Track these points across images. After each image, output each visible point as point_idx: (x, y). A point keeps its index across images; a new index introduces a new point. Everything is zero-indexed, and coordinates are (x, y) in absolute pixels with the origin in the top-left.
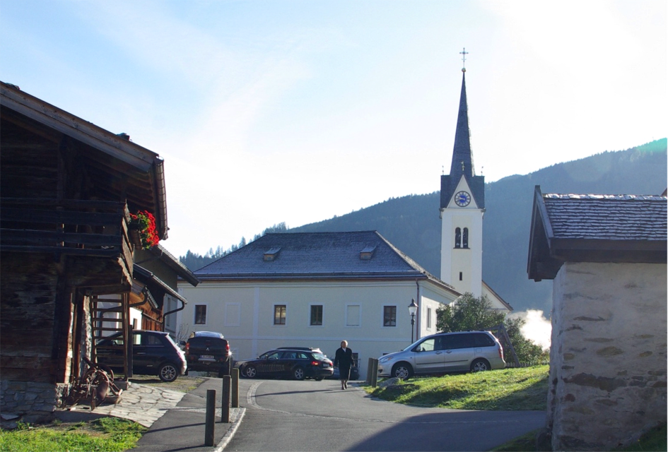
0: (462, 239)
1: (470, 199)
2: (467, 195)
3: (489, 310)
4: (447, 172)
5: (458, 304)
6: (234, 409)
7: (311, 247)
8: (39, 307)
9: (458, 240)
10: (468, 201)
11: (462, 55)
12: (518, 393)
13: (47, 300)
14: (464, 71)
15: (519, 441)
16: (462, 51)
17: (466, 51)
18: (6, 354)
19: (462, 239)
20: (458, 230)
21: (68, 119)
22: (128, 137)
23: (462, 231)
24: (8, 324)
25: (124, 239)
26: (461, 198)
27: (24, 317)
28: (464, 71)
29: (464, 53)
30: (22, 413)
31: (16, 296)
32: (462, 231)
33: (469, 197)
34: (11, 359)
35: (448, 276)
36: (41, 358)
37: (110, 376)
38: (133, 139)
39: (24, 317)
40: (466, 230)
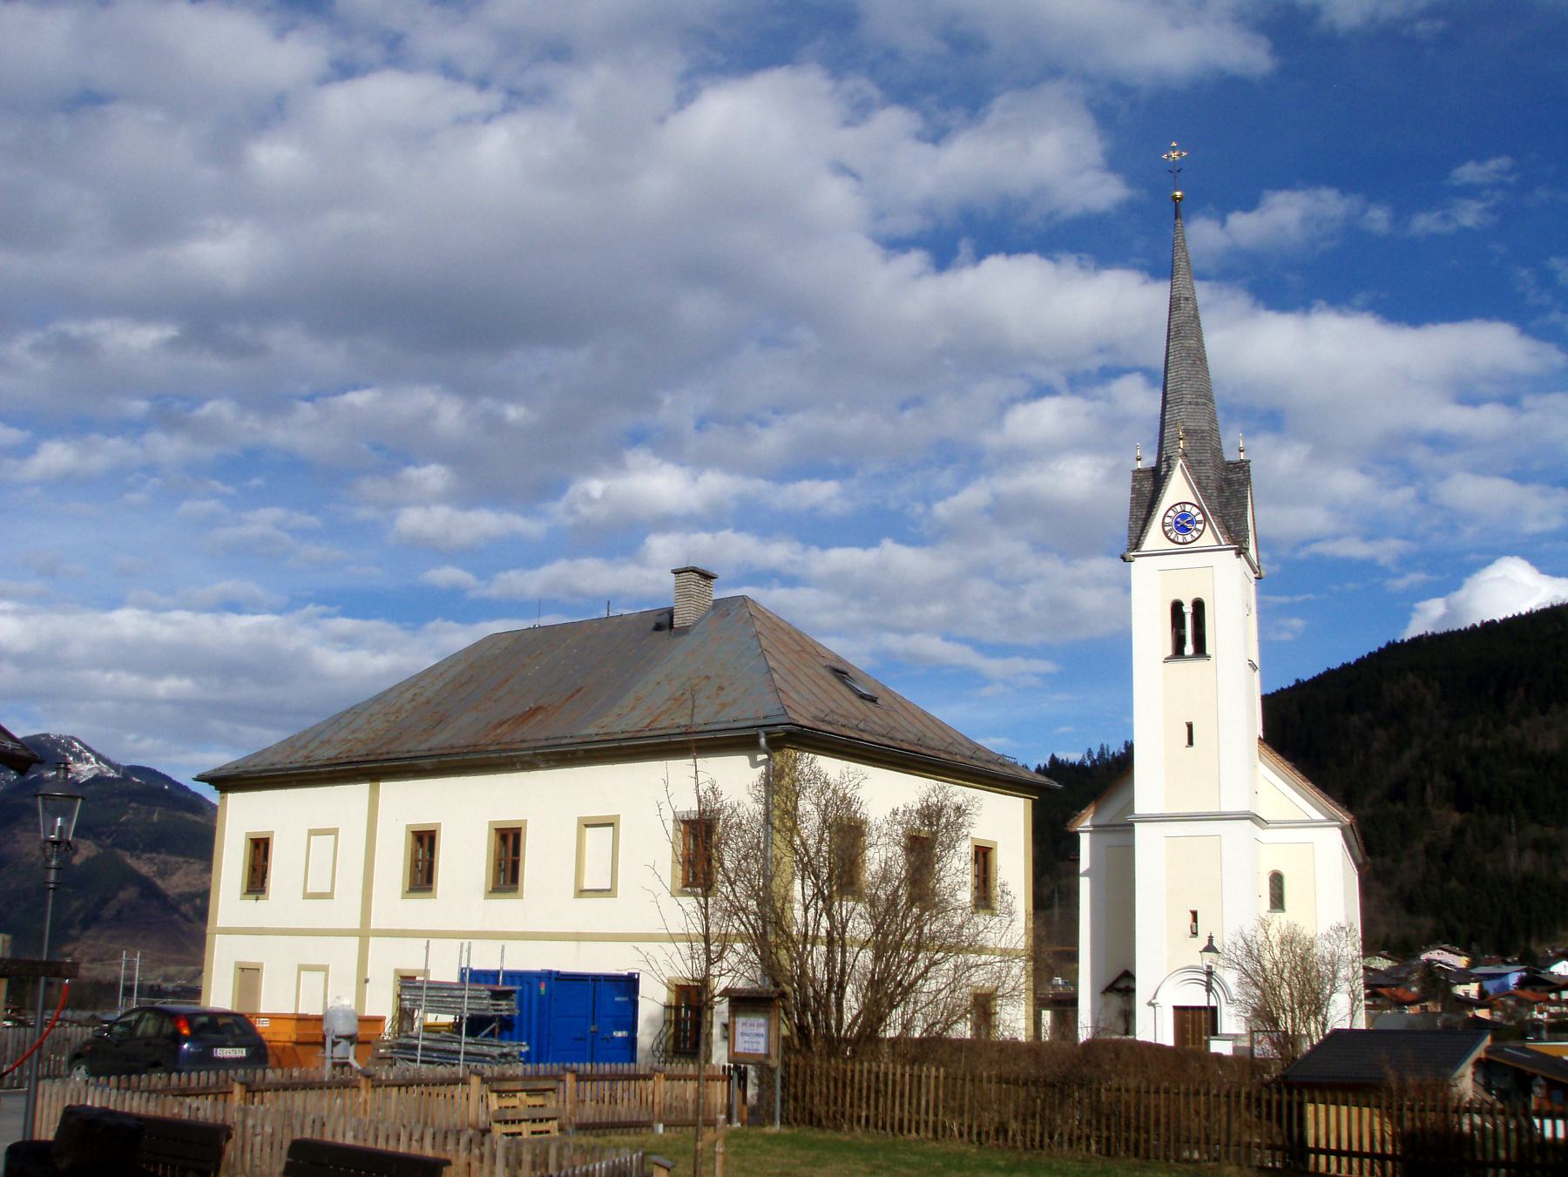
20: (1177, 607)
23: (1188, 609)
32: (1188, 609)
40: (1198, 606)
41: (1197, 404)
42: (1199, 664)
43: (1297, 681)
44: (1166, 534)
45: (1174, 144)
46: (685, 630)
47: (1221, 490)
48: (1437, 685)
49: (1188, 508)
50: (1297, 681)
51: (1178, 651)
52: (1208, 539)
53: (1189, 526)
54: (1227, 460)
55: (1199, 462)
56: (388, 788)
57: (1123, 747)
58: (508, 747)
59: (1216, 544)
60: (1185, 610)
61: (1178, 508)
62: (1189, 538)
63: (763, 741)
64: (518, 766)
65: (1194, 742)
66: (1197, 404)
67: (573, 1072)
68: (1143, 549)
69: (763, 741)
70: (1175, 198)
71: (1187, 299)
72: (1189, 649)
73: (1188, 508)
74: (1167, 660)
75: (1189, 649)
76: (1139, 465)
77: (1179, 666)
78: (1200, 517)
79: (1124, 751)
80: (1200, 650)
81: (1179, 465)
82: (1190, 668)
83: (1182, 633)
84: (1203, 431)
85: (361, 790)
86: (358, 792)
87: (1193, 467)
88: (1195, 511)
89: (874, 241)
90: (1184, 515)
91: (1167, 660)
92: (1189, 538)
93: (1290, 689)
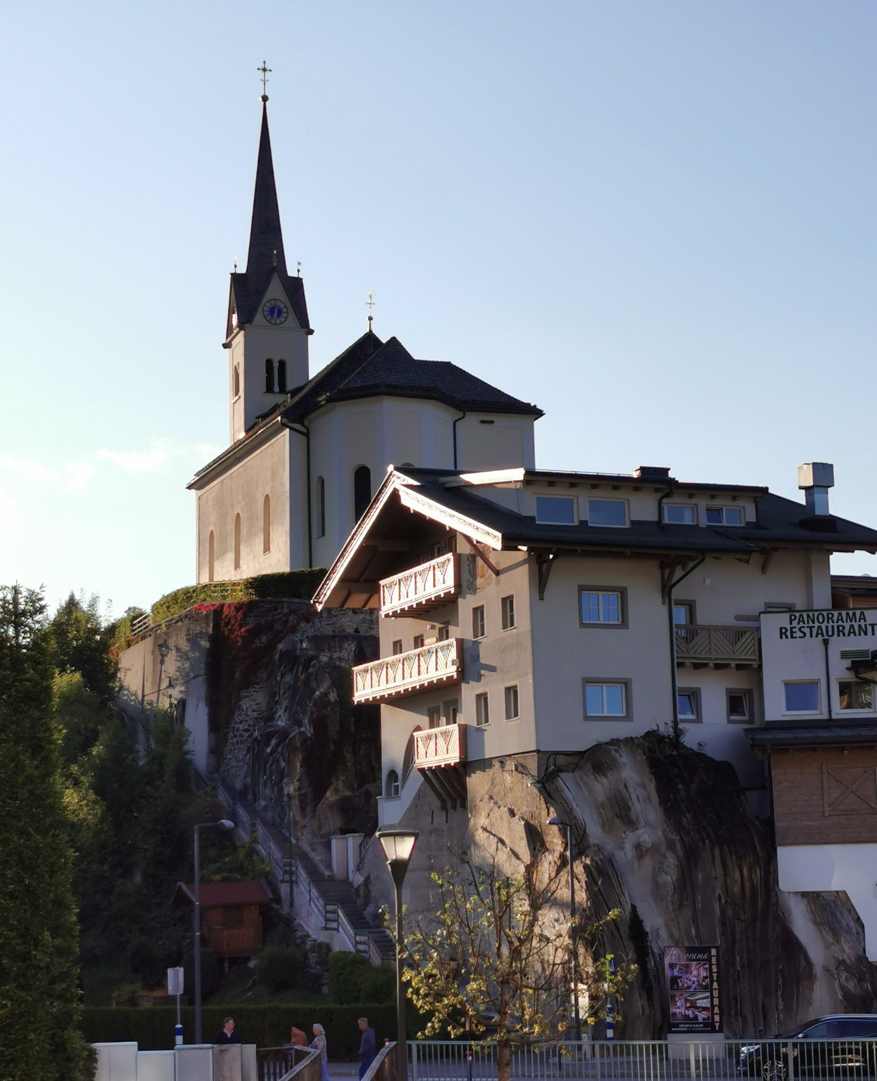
1: (287, 313)
2: (282, 306)
4: (242, 269)
6: (568, 1062)
10: (285, 315)
11: (261, 73)
14: (265, 99)
15: (153, 607)
16: (261, 66)
17: (268, 67)
20: (269, 363)
21: (849, 549)
22: (767, 488)
23: (276, 365)
25: (802, 958)
26: (275, 315)
28: (265, 99)
29: (264, 70)
32: (276, 365)
33: (285, 310)
38: (681, 474)
40: (282, 364)
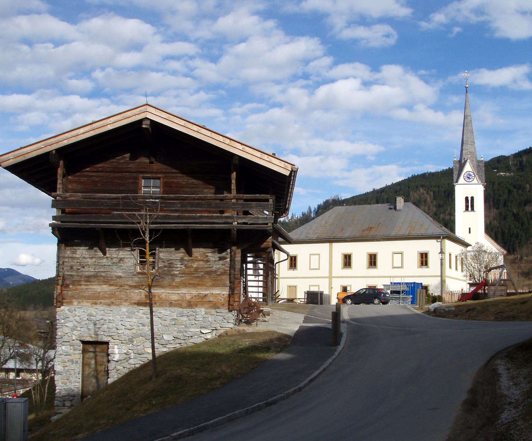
0: (470, 204)
3: (137, 243)
5: (233, 249)
7: (508, 369)
8: (221, 262)
9: (467, 207)
12: (259, 197)
13: (225, 258)
18: (202, 292)
19: (470, 204)
20: (467, 198)
23: (470, 199)
24: (203, 273)
27: (212, 269)
30: (214, 329)
31: (207, 256)
32: (470, 199)
34: (206, 295)
35: (460, 232)
36: (224, 295)
37: (35, 396)
39: (212, 269)
40: (472, 198)
41: (472, 145)
42: (472, 213)
43: (374, 189)
44: (464, 179)
45: (466, 72)
46: (400, 210)
47: (477, 168)
48: (432, 193)
49: (470, 173)
50: (374, 189)
51: (467, 209)
52: (475, 181)
53: (471, 178)
54: (478, 160)
55: (472, 160)
56: (334, 244)
57: (301, 214)
58: (375, 236)
59: (477, 182)
60: (469, 199)
61: (468, 173)
62: (470, 181)
63: (442, 237)
64: (375, 241)
65: (471, 232)
66: (472, 145)
67: (526, 285)
68: (458, 183)
69: (442, 237)
70: (466, 87)
71: (469, 116)
72: (470, 209)
73: (470, 173)
74: (464, 212)
75: (470, 209)
76: (455, 159)
77: (467, 213)
78: (473, 175)
79: (302, 216)
80: (473, 209)
81: (468, 162)
82: (470, 214)
83: (494, 212)
84: (473, 152)
85: (327, 245)
86: (325, 246)
87: (472, 161)
88: (472, 174)
89: (286, 44)
90: (470, 175)
91: (464, 212)
92: (470, 181)
93: (372, 192)
